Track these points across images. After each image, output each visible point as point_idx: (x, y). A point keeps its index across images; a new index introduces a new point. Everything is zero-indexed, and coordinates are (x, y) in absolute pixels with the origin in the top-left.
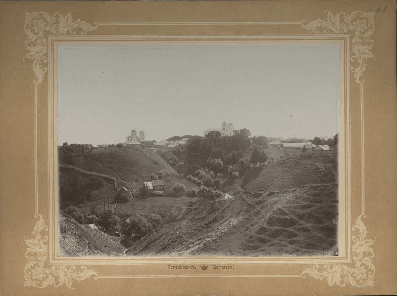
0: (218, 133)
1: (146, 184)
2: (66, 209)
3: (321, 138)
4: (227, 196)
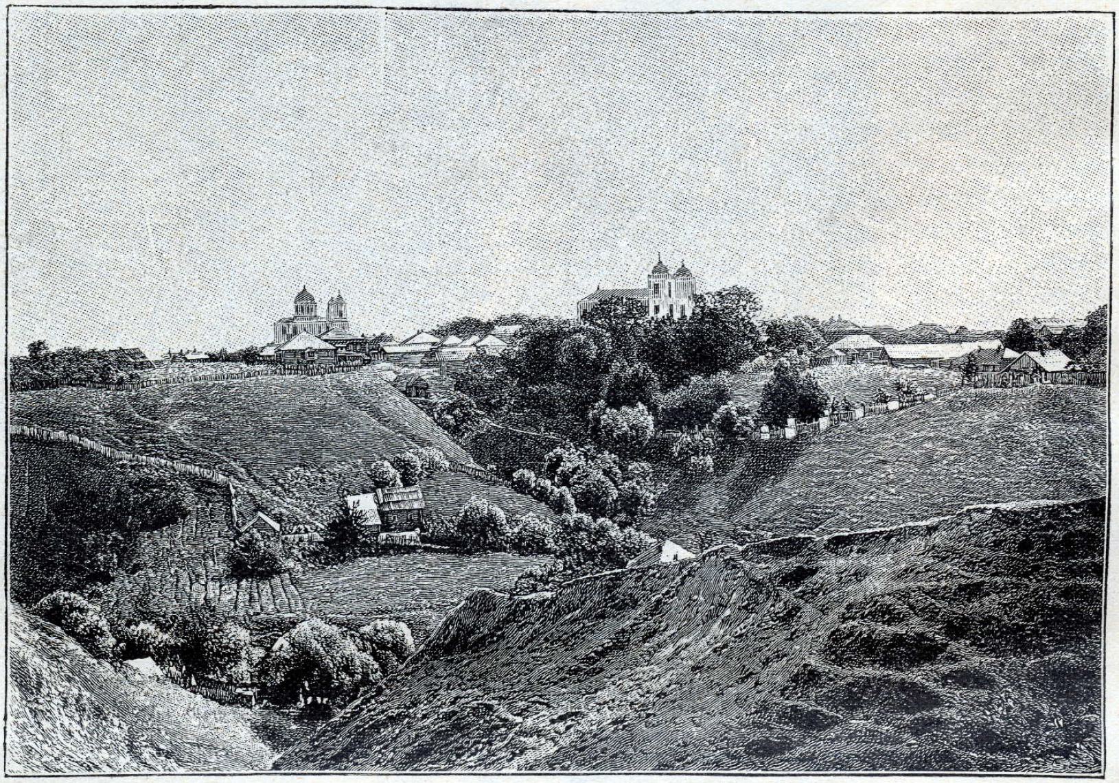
0: (636, 307)
1: (350, 505)
2: (44, 600)
3: (1034, 326)
4: (671, 552)
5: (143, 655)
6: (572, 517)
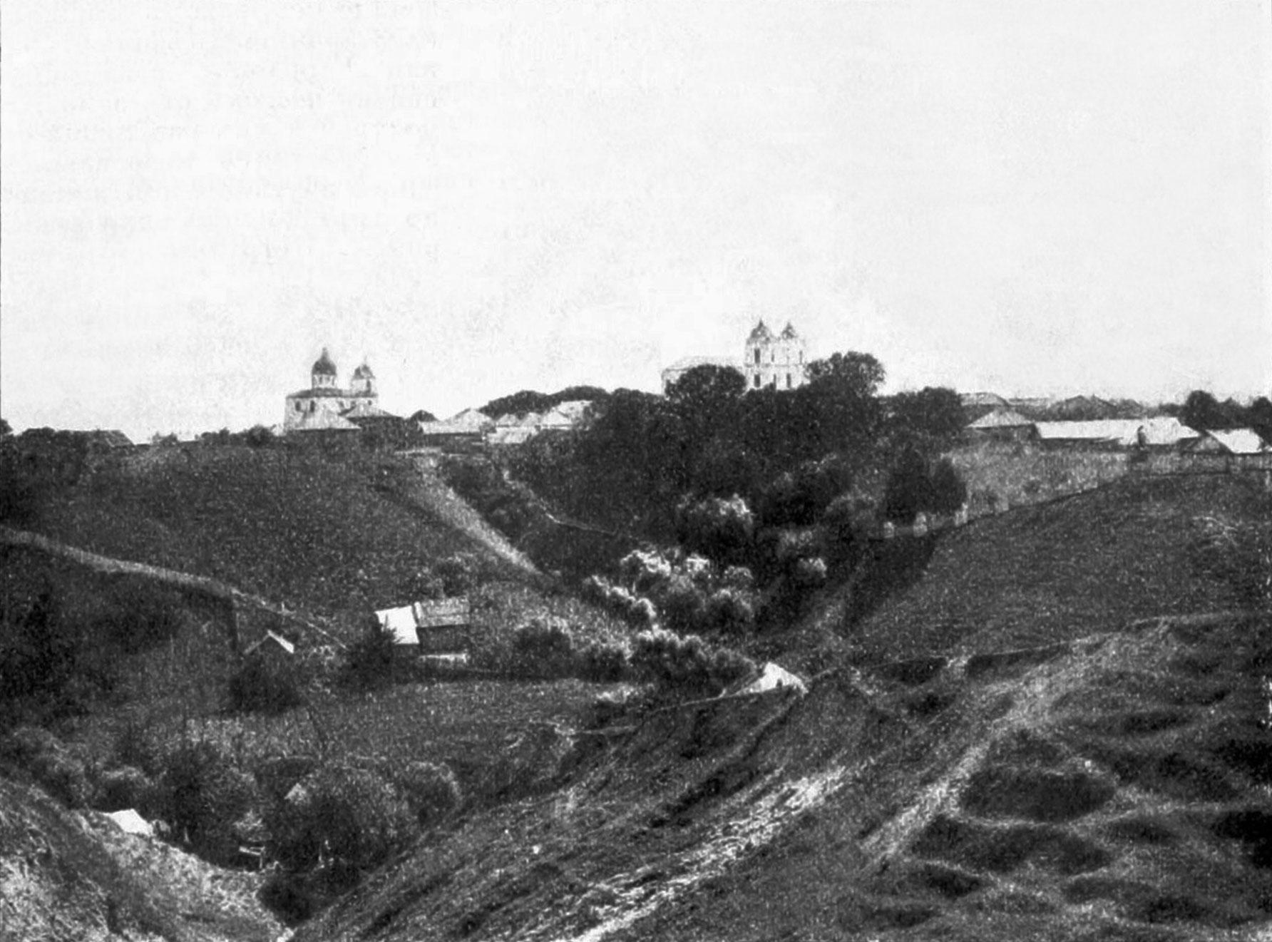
0: (730, 377)
1: (382, 620)
4: (773, 676)
5: (125, 806)
6: (655, 633)
